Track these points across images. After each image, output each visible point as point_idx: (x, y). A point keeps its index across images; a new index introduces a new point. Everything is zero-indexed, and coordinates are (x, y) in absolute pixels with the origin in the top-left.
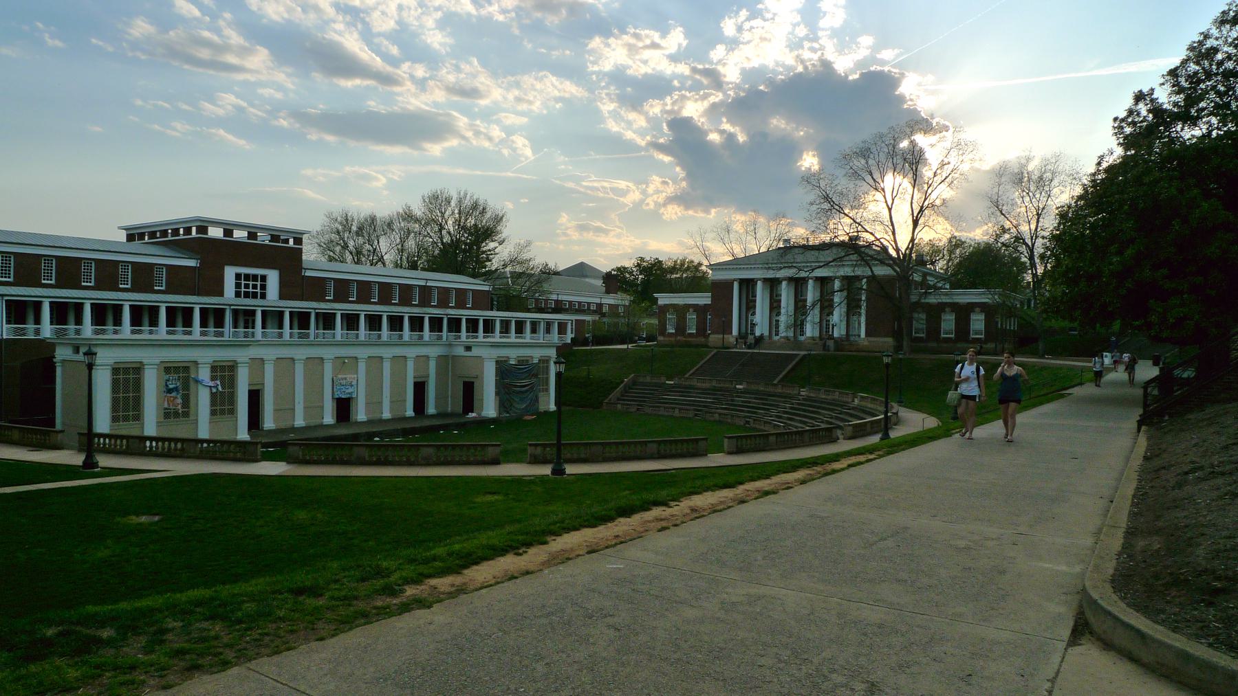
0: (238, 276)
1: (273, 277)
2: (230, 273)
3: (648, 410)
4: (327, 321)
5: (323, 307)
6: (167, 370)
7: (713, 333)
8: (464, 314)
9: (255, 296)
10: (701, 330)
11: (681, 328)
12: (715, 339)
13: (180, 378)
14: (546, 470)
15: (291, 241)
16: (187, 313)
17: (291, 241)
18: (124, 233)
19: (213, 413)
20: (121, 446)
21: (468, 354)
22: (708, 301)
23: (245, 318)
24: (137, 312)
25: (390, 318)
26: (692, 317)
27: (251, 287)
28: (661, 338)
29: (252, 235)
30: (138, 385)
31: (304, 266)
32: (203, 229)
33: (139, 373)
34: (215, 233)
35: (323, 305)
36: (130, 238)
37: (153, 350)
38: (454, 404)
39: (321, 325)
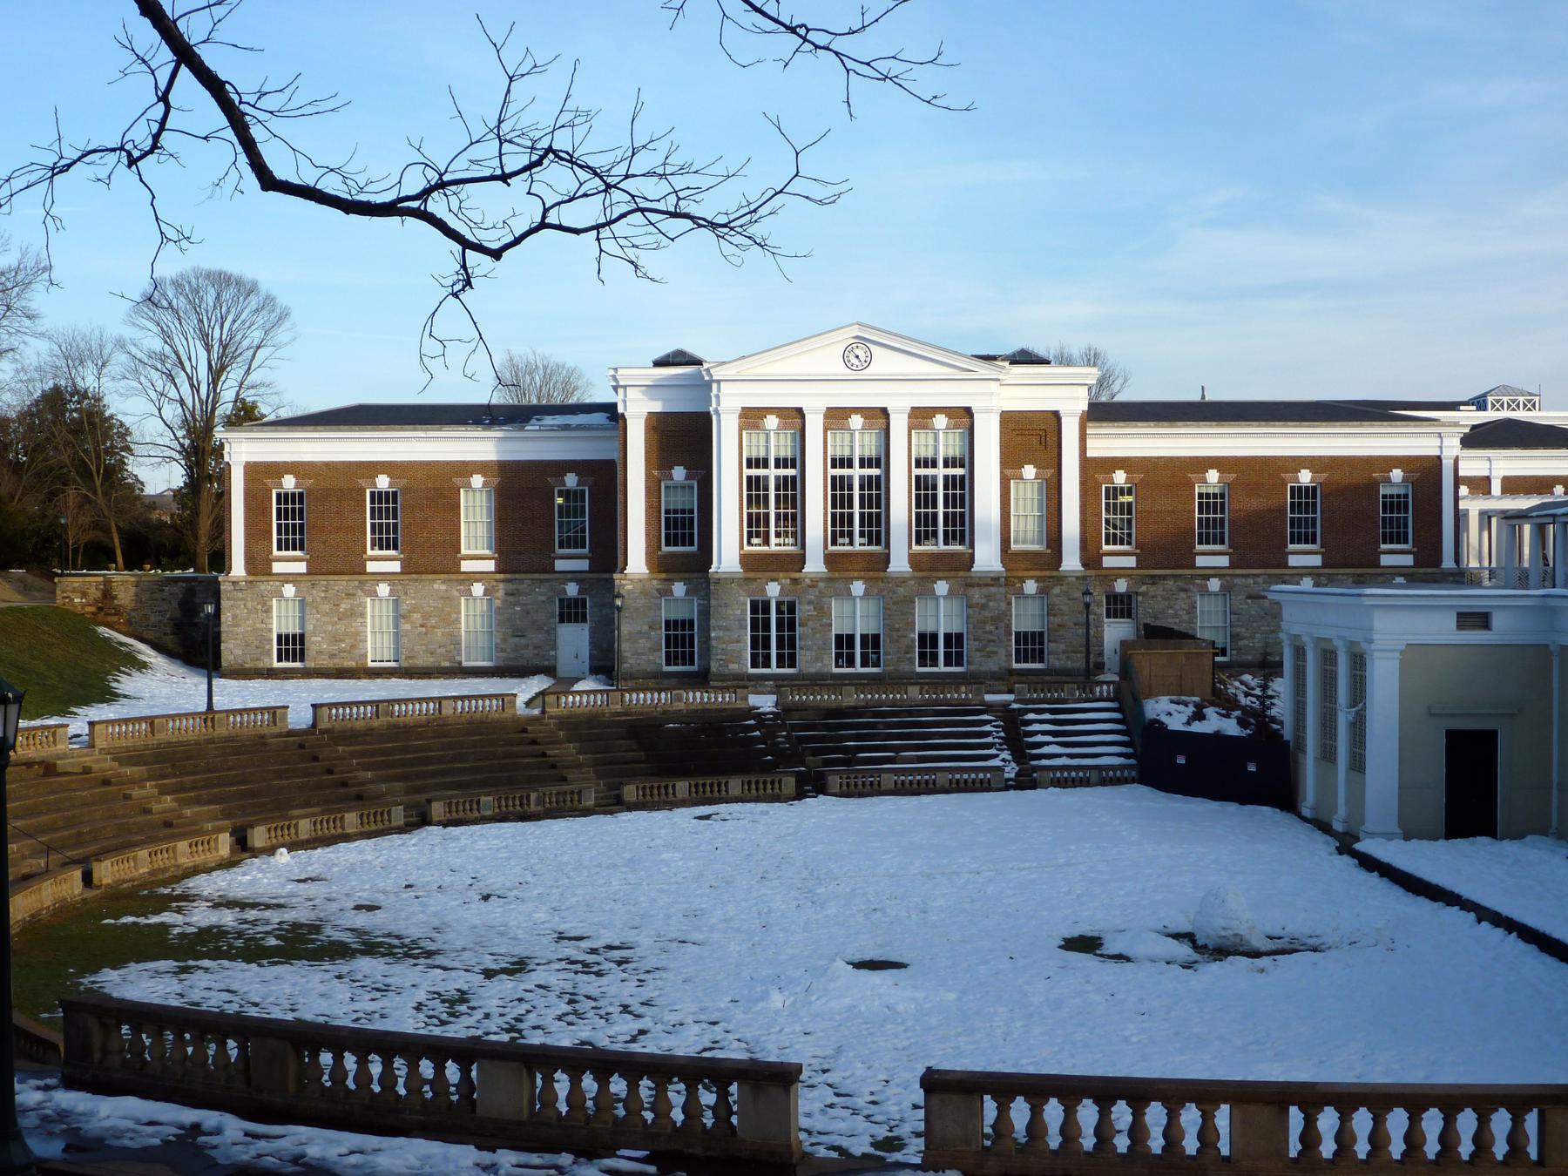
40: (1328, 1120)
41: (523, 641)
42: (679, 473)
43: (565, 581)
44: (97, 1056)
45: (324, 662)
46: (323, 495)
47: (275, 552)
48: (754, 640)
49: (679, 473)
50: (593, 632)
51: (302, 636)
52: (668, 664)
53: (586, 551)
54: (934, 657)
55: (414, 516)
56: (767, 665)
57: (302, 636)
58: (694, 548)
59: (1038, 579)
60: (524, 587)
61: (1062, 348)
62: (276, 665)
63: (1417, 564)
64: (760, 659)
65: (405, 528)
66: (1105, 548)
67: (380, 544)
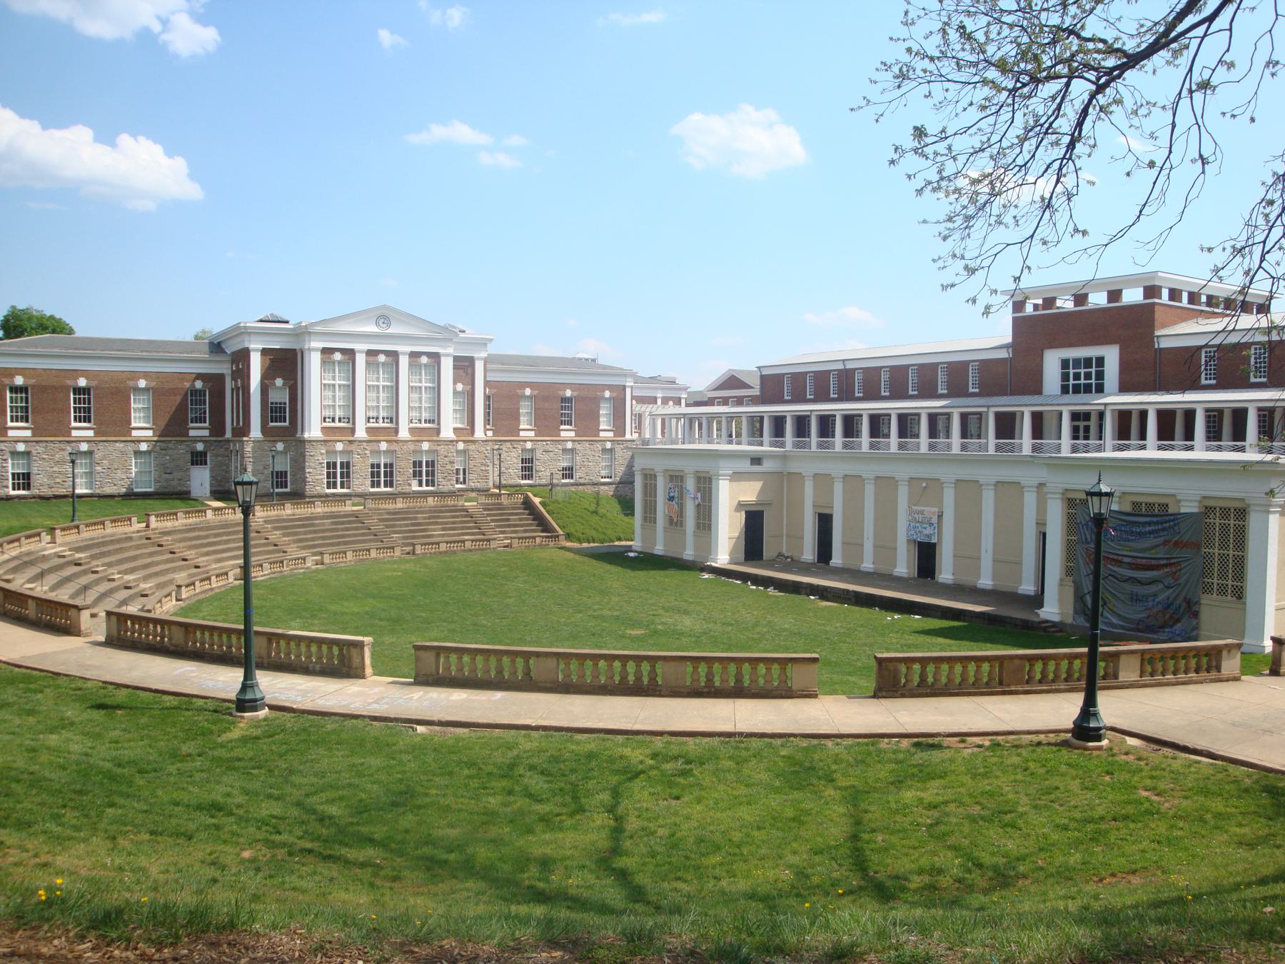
1: (1111, 355)
2: (1052, 361)
9: (1088, 389)
16: (1239, 415)
29: (1114, 295)
40: (631, 667)
41: (171, 477)
42: (279, 382)
43: (196, 441)
44: (903, 681)
45: (47, 492)
46: (42, 389)
47: (10, 424)
48: (328, 474)
49: (279, 382)
50: (212, 470)
51: (29, 474)
52: (373, 486)
53: (207, 425)
54: (335, 484)
55: (102, 404)
56: (379, 486)
57: (29, 474)
58: (287, 424)
59: (464, 441)
60: (170, 445)
61: (13, 307)
62: (12, 493)
63: (96, 434)
64: (332, 485)
65: (97, 409)
66: (74, 424)
67: (78, 419)
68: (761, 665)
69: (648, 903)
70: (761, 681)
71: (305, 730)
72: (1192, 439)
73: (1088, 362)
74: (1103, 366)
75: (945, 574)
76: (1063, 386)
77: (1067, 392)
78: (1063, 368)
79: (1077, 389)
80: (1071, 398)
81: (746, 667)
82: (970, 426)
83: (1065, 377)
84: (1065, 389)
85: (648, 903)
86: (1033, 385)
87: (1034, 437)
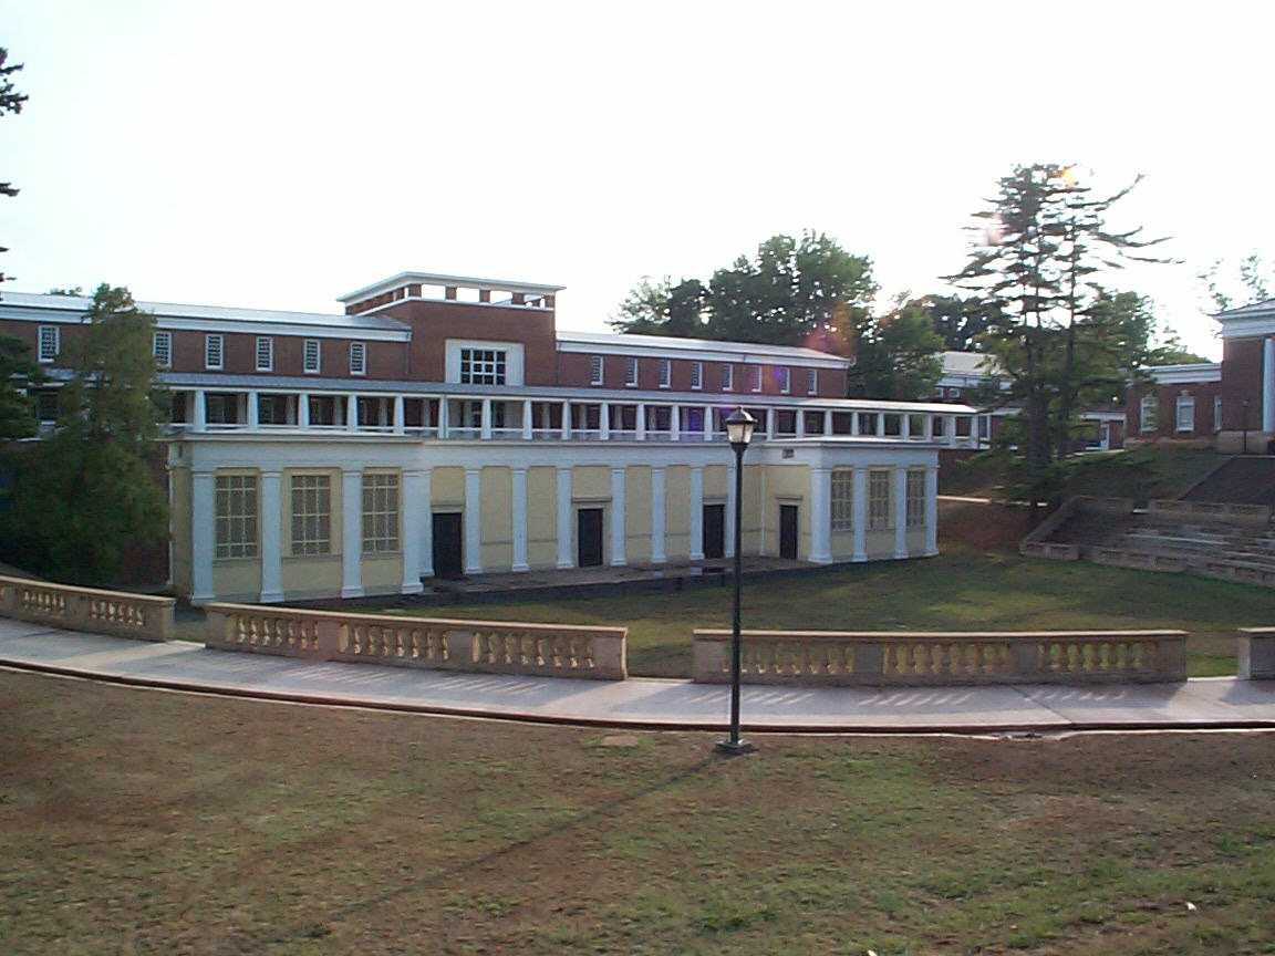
0: (465, 354)
1: (515, 355)
2: (453, 351)
3: (1101, 560)
4: (587, 416)
5: (583, 396)
6: (296, 480)
7: (1222, 430)
8: (771, 404)
9: (489, 380)
10: (1204, 423)
11: (1167, 425)
12: (1229, 439)
13: (312, 494)
14: (742, 632)
15: (543, 302)
16: (556, 409)
17: (543, 302)
18: (343, 306)
19: (366, 546)
20: (1064, 663)
21: (788, 461)
22: (1219, 379)
23: (466, 413)
24: (499, 410)
25: (808, 415)
26: (1186, 403)
27: (486, 370)
28: (1131, 441)
29: (518, 299)
30: (253, 502)
31: (559, 337)
32: (415, 289)
33: (254, 485)
34: (434, 293)
35: (691, 397)
36: (350, 311)
37: (348, 453)
38: (766, 542)
39: (686, 425)
68: (1088, 646)
69: (1199, 889)
70: (1088, 666)
71: (191, 765)
72: (436, 425)
73: (489, 355)
74: (504, 360)
75: (617, 552)
76: (463, 376)
77: (468, 382)
78: (464, 358)
79: (478, 380)
80: (471, 386)
81: (1088, 650)
82: (660, 418)
83: (465, 367)
84: (465, 380)
85: (1199, 889)
86: (436, 372)
87: (611, 428)
